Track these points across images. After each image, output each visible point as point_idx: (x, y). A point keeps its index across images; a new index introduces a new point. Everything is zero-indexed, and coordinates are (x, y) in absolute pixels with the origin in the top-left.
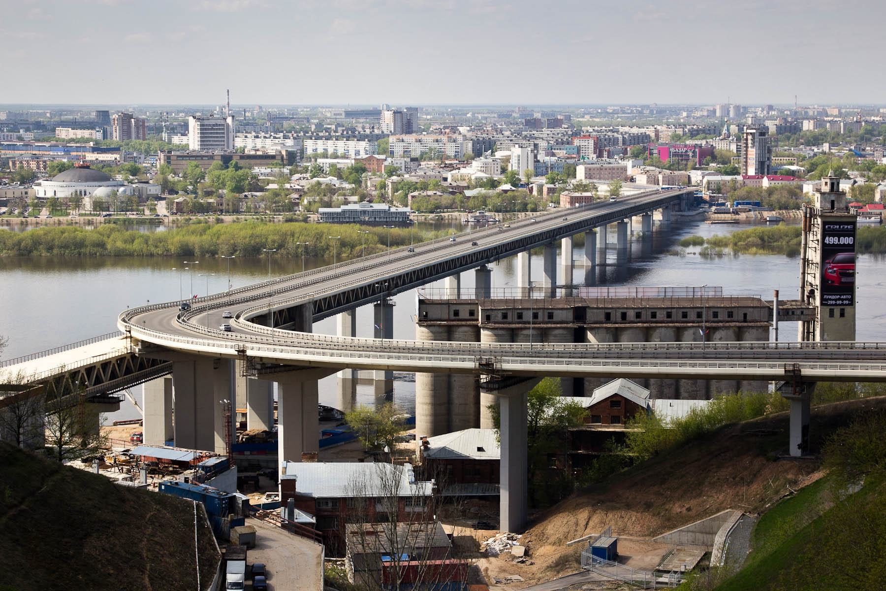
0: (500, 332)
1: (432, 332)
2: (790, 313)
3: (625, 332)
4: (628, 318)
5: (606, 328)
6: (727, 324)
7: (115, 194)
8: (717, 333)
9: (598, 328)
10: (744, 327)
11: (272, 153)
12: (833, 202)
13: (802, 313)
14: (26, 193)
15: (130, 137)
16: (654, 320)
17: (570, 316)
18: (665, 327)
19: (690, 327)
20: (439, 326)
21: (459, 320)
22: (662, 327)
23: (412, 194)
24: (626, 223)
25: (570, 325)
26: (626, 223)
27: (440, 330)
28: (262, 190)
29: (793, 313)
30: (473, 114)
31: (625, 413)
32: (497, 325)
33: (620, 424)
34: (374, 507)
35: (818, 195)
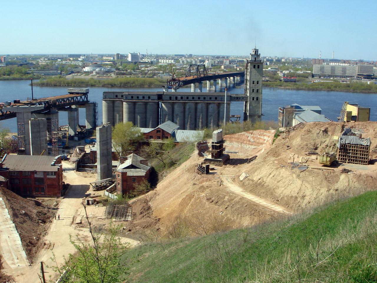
0: (129, 103)
1: (107, 103)
2: (239, 98)
5: (169, 102)
8: (210, 105)
9: (166, 102)
10: (220, 103)
12: (255, 58)
13: (243, 98)
15: (119, 59)
17: (156, 97)
18: (191, 102)
20: (142, 102)
21: (139, 100)
24: (227, 79)
26: (227, 79)
27: (110, 102)
28: (140, 70)
29: (240, 98)
32: (129, 101)
33: (160, 140)
34: (34, 175)
35: (250, 56)
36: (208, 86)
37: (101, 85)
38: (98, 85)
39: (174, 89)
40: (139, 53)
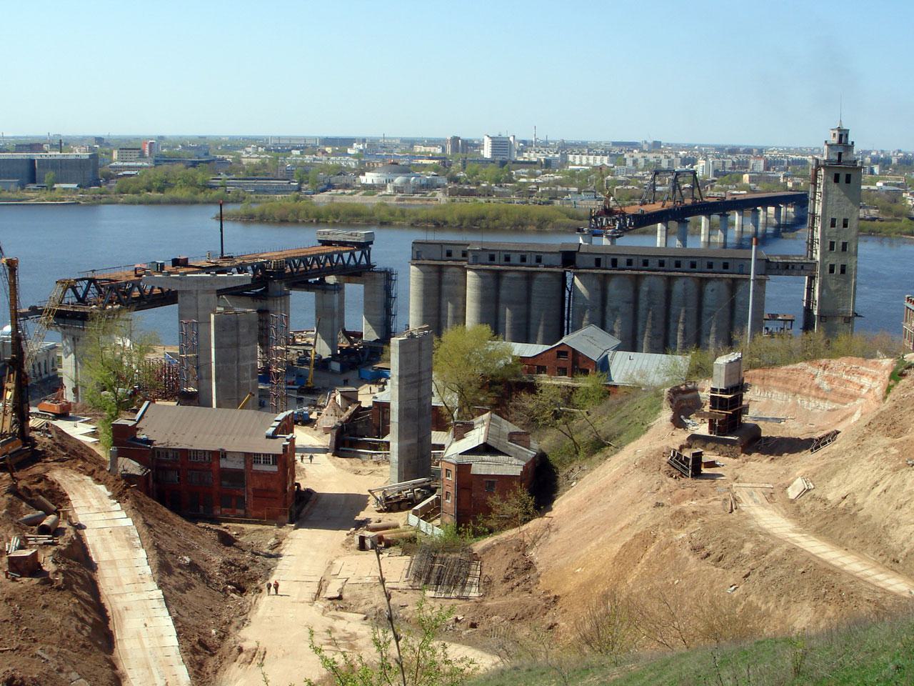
1: (480, 277)
2: (790, 267)
3: (613, 279)
4: (619, 266)
6: (720, 276)
7: (408, 181)
10: (737, 279)
11: (535, 160)
13: (802, 268)
14: (355, 181)
16: (711, 270)
18: (655, 275)
19: (680, 277)
22: (651, 275)
23: (617, 188)
25: (555, 270)
27: (430, 269)
29: (793, 267)
30: (699, 148)
31: (572, 366)
36: (703, 232)
37: (406, 224)
38: (397, 223)
39: (607, 237)
40: (514, 136)
